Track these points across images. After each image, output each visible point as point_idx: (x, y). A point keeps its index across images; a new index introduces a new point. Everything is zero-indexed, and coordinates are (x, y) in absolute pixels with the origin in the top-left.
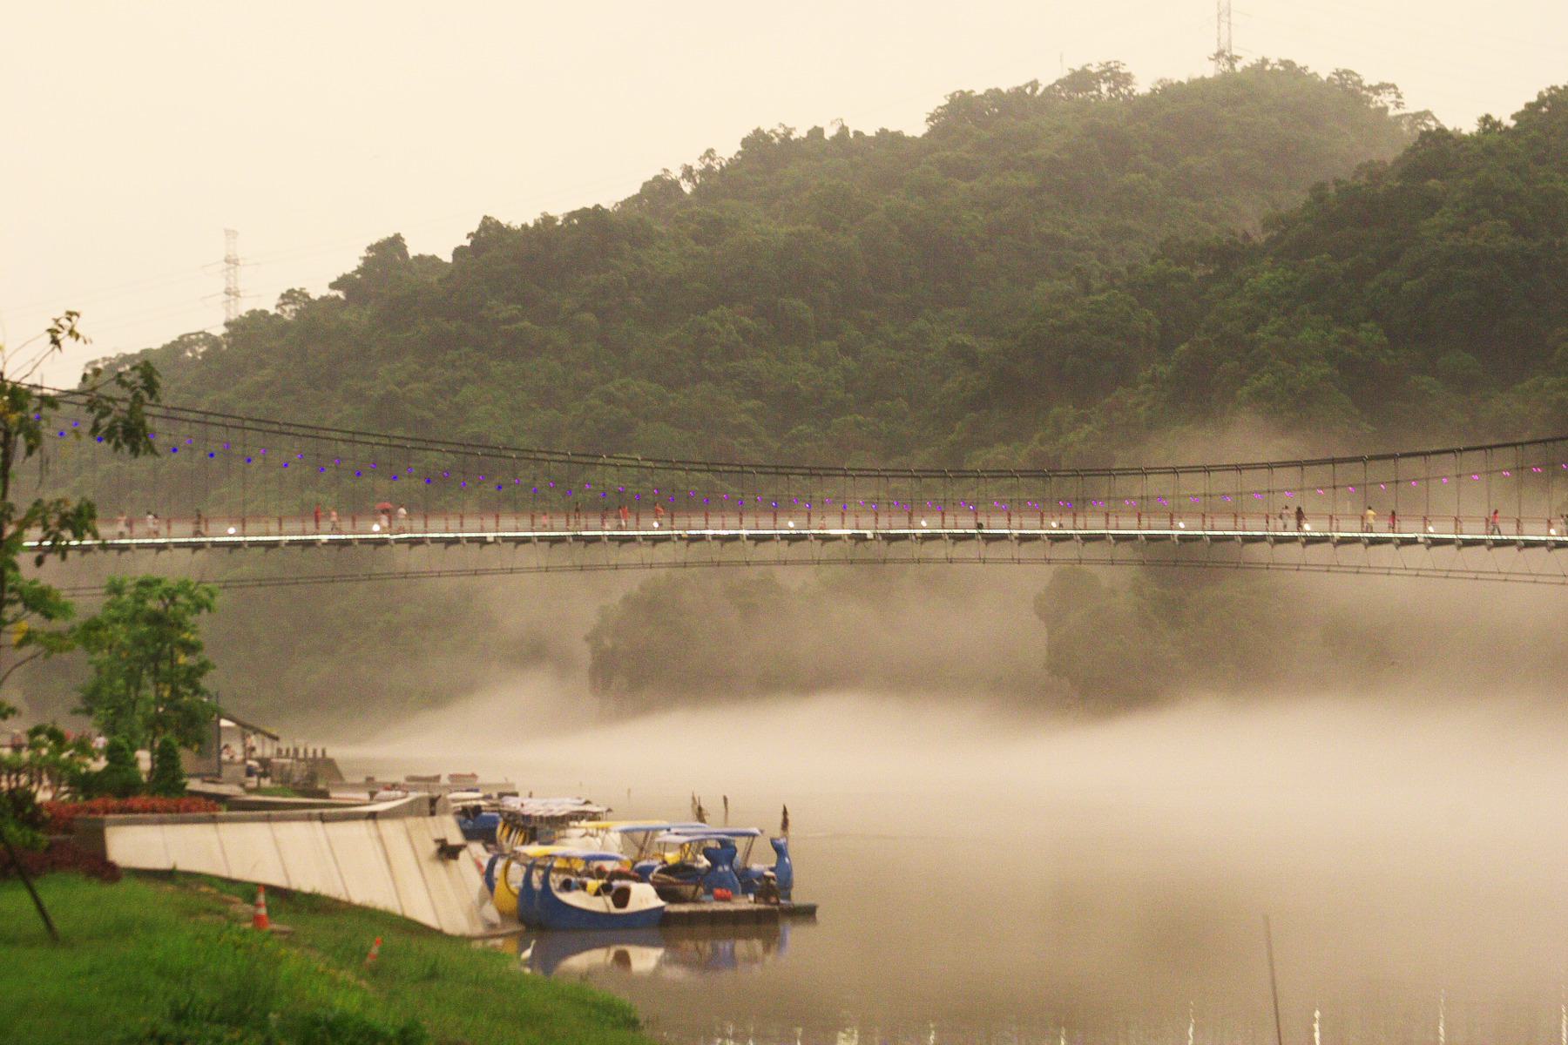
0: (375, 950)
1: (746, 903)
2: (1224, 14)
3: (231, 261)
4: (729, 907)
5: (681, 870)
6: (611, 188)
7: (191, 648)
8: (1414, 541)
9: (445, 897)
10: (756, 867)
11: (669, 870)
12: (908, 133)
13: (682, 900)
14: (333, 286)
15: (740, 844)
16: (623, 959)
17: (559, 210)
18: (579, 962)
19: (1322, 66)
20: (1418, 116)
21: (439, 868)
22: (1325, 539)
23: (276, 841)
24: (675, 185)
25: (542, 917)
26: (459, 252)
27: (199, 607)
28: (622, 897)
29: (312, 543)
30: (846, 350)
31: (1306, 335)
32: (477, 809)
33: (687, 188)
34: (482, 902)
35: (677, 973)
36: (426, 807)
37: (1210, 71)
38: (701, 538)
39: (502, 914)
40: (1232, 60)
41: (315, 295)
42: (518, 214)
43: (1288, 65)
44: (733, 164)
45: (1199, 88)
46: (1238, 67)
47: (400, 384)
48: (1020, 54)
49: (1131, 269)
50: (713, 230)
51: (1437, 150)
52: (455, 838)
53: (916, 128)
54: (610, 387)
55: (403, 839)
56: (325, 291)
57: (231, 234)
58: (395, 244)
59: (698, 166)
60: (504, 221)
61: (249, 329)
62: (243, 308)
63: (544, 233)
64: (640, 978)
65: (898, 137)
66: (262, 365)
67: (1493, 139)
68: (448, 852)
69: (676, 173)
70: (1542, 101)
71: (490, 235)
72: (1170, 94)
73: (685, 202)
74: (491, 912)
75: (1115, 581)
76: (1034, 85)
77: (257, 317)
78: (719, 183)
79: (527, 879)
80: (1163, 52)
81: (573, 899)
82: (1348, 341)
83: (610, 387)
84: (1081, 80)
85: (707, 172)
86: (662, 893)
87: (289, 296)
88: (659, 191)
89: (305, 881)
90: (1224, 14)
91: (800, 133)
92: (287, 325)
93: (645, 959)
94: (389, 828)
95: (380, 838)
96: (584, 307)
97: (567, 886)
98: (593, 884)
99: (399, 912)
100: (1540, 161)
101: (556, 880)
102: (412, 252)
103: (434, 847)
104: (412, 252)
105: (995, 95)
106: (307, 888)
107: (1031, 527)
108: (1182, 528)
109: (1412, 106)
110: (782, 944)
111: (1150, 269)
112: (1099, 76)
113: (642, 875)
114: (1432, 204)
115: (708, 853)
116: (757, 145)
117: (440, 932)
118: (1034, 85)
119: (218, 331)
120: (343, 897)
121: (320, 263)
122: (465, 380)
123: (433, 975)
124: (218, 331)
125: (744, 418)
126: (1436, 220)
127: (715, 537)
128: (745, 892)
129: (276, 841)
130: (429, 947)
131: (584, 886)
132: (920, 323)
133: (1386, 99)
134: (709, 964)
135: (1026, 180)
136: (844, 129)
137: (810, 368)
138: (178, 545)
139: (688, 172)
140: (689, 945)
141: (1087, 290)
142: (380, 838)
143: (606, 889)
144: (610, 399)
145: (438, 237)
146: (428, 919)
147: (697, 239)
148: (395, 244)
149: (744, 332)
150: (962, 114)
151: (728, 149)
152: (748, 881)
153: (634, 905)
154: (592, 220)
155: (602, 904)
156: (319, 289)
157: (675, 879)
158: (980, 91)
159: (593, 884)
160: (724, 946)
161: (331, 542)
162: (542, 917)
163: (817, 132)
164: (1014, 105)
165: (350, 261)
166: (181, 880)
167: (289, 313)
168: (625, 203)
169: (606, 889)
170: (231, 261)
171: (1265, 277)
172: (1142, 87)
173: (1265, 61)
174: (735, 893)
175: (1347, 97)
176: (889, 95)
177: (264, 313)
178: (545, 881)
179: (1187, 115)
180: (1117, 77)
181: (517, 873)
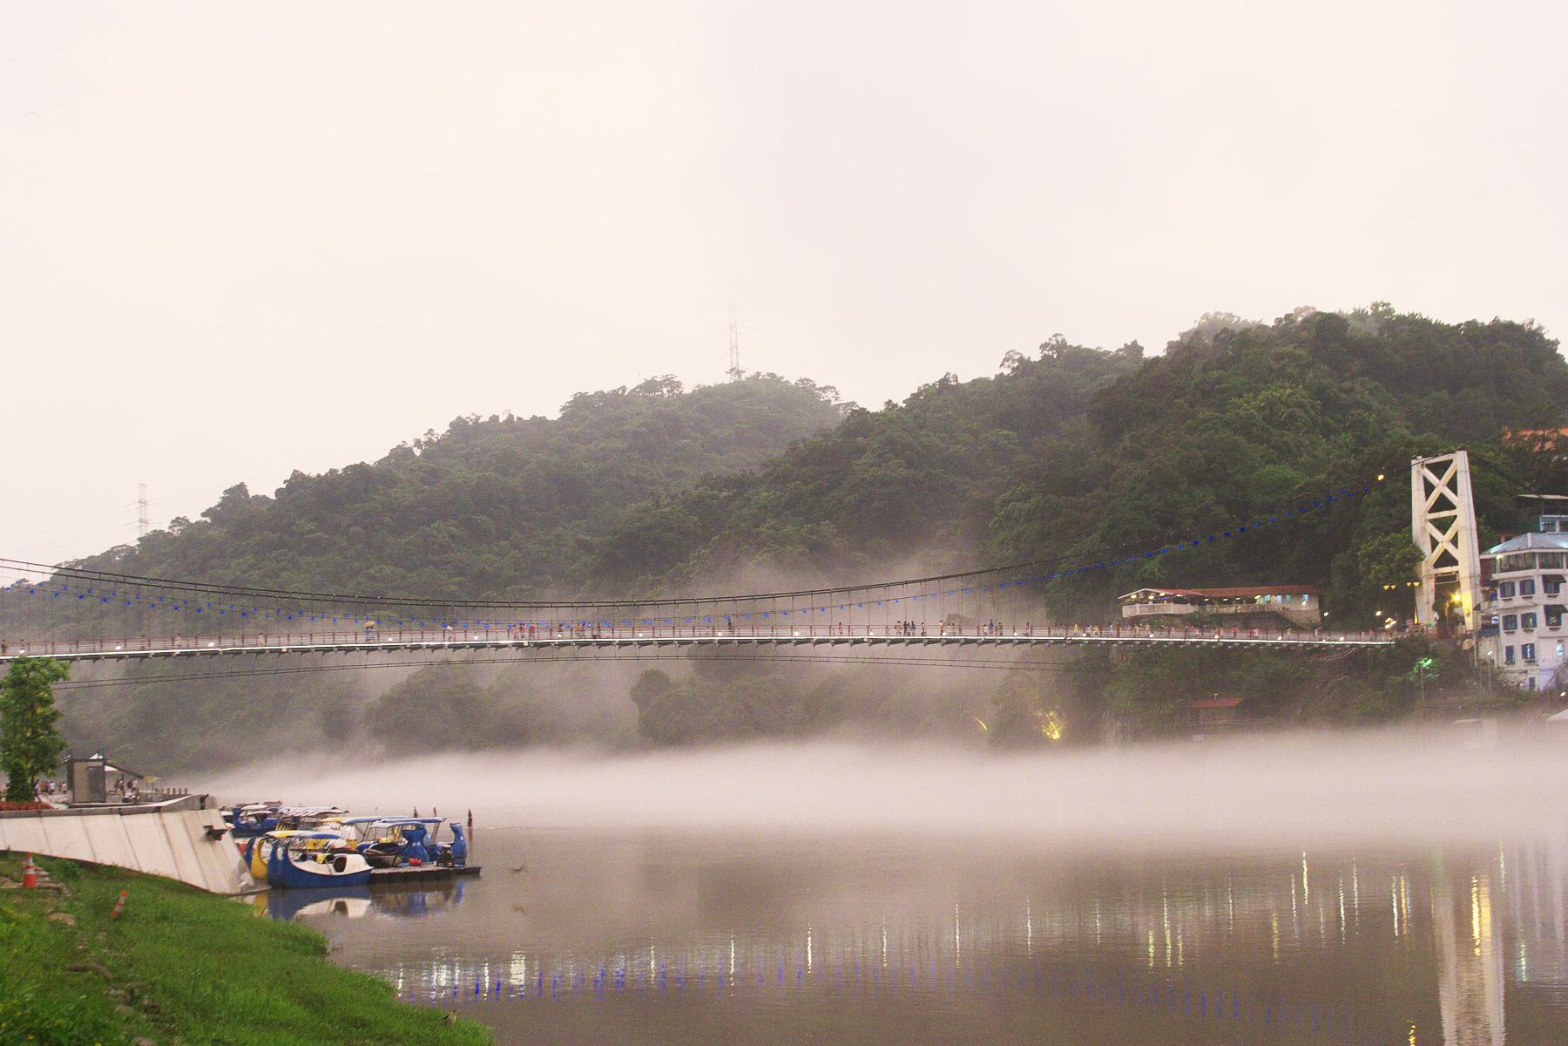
0: (122, 900)
1: (432, 867)
2: (734, 348)
3: (143, 503)
4: (418, 869)
5: (390, 848)
6: (373, 453)
7: (47, 702)
8: (861, 641)
9: (218, 869)
10: (440, 844)
11: (381, 846)
12: (549, 418)
13: (386, 866)
14: (203, 515)
15: (429, 828)
16: (342, 908)
17: (340, 466)
18: (310, 910)
19: (792, 377)
20: (847, 405)
21: (208, 846)
22: (807, 641)
23: (86, 830)
24: (410, 450)
25: (286, 883)
26: (279, 492)
27: (57, 677)
28: (341, 864)
29: (169, 655)
30: (515, 547)
31: (789, 529)
32: (265, 816)
33: (417, 452)
34: (242, 871)
35: (388, 918)
36: (197, 803)
37: (727, 380)
38: (419, 647)
39: (256, 879)
40: (739, 373)
41: (193, 521)
42: (316, 468)
43: (772, 375)
44: (445, 439)
45: (720, 390)
46: (743, 377)
47: (245, 572)
48: (616, 371)
49: (683, 493)
50: (432, 476)
51: (860, 420)
52: (219, 824)
53: (554, 415)
54: (372, 571)
55: (181, 827)
56: (200, 518)
57: (143, 486)
58: (241, 489)
59: (423, 439)
60: (306, 473)
61: (152, 542)
62: (149, 529)
63: (331, 480)
64: (357, 921)
65: (543, 420)
66: (160, 562)
67: (893, 415)
68: (213, 835)
69: (410, 444)
70: (920, 393)
71: (298, 482)
72: (704, 393)
73: (417, 460)
74: (247, 879)
75: (679, 670)
76: (624, 389)
77: (157, 534)
78: (436, 449)
79: (274, 853)
80: (699, 369)
81: (307, 866)
82: (812, 532)
83: (372, 571)
84: (651, 386)
85: (429, 442)
86: (369, 862)
87: (177, 521)
88: (401, 454)
89: (106, 858)
90: (734, 348)
91: (485, 419)
92: (176, 539)
93: (358, 907)
94: (169, 818)
95: (164, 826)
96: (355, 524)
97: (304, 858)
98: (321, 856)
99: (176, 877)
100: (921, 427)
101: (293, 856)
102: (251, 494)
103: (204, 832)
104: (251, 494)
105: (601, 395)
106: (108, 862)
107: (626, 636)
108: (720, 635)
109: (844, 399)
110: (459, 896)
111: (695, 493)
112: (661, 384)
113: (360, 850)
114: (860, 451)
115: (405, 834)
116: (459, 426)
117: (205, 892)
118: (624, 389)
119: (134, 543)
120: (136, 868)
121: (194, 501)
122: (283, 569)
123: (164, 918)
124: (134, 543)
125: (454, 588)
126: (862, 461)
127: (428, 647)
128: (432, 860)
129: (86, 830)
130: (186, 902)
131: (315, 858)
132: (559, 530)
133: (829, 395)
134: (409, 909)
135: (620, 444)
136: (511, 416)
137: (493, 557)
138: (84, 658)
139: (418, 443)
140: (390, 897)
141: (658, 506)
142: (164, 826)
143: (329, 859)
144: (373, 578)
145: (266, 484)
146: (198, 882)
147: (424, 481)
148: (241, 489)
149: (453, 537)
150: (581, 406)
151: (442, 429)
152: (433, 853)
153: (348, 870)
154: (359, 472)
155: (326, 869)
156: (195, 517)
157: (378, 854)
158: (591, 393)
159: (321, 856)
160: (418, 897)
161: (181, 654)
162: (286, 883)
163: (495, 418)
164: (613, 400)
165: (214, 500)
166: (12, 857)
167: (176, 531)
168: (380, 462)
169: (329, 859)
170: (143, 503)
171: (764, 495)
172: (687, 389)
173: (758, 374)
174: (424, 861)
175: (805, 395)
176: (540, 398)
177: (161, 532)
178: (285, 854)
179: (713, 406)
180: (672, 384)
181: (267, 849)
